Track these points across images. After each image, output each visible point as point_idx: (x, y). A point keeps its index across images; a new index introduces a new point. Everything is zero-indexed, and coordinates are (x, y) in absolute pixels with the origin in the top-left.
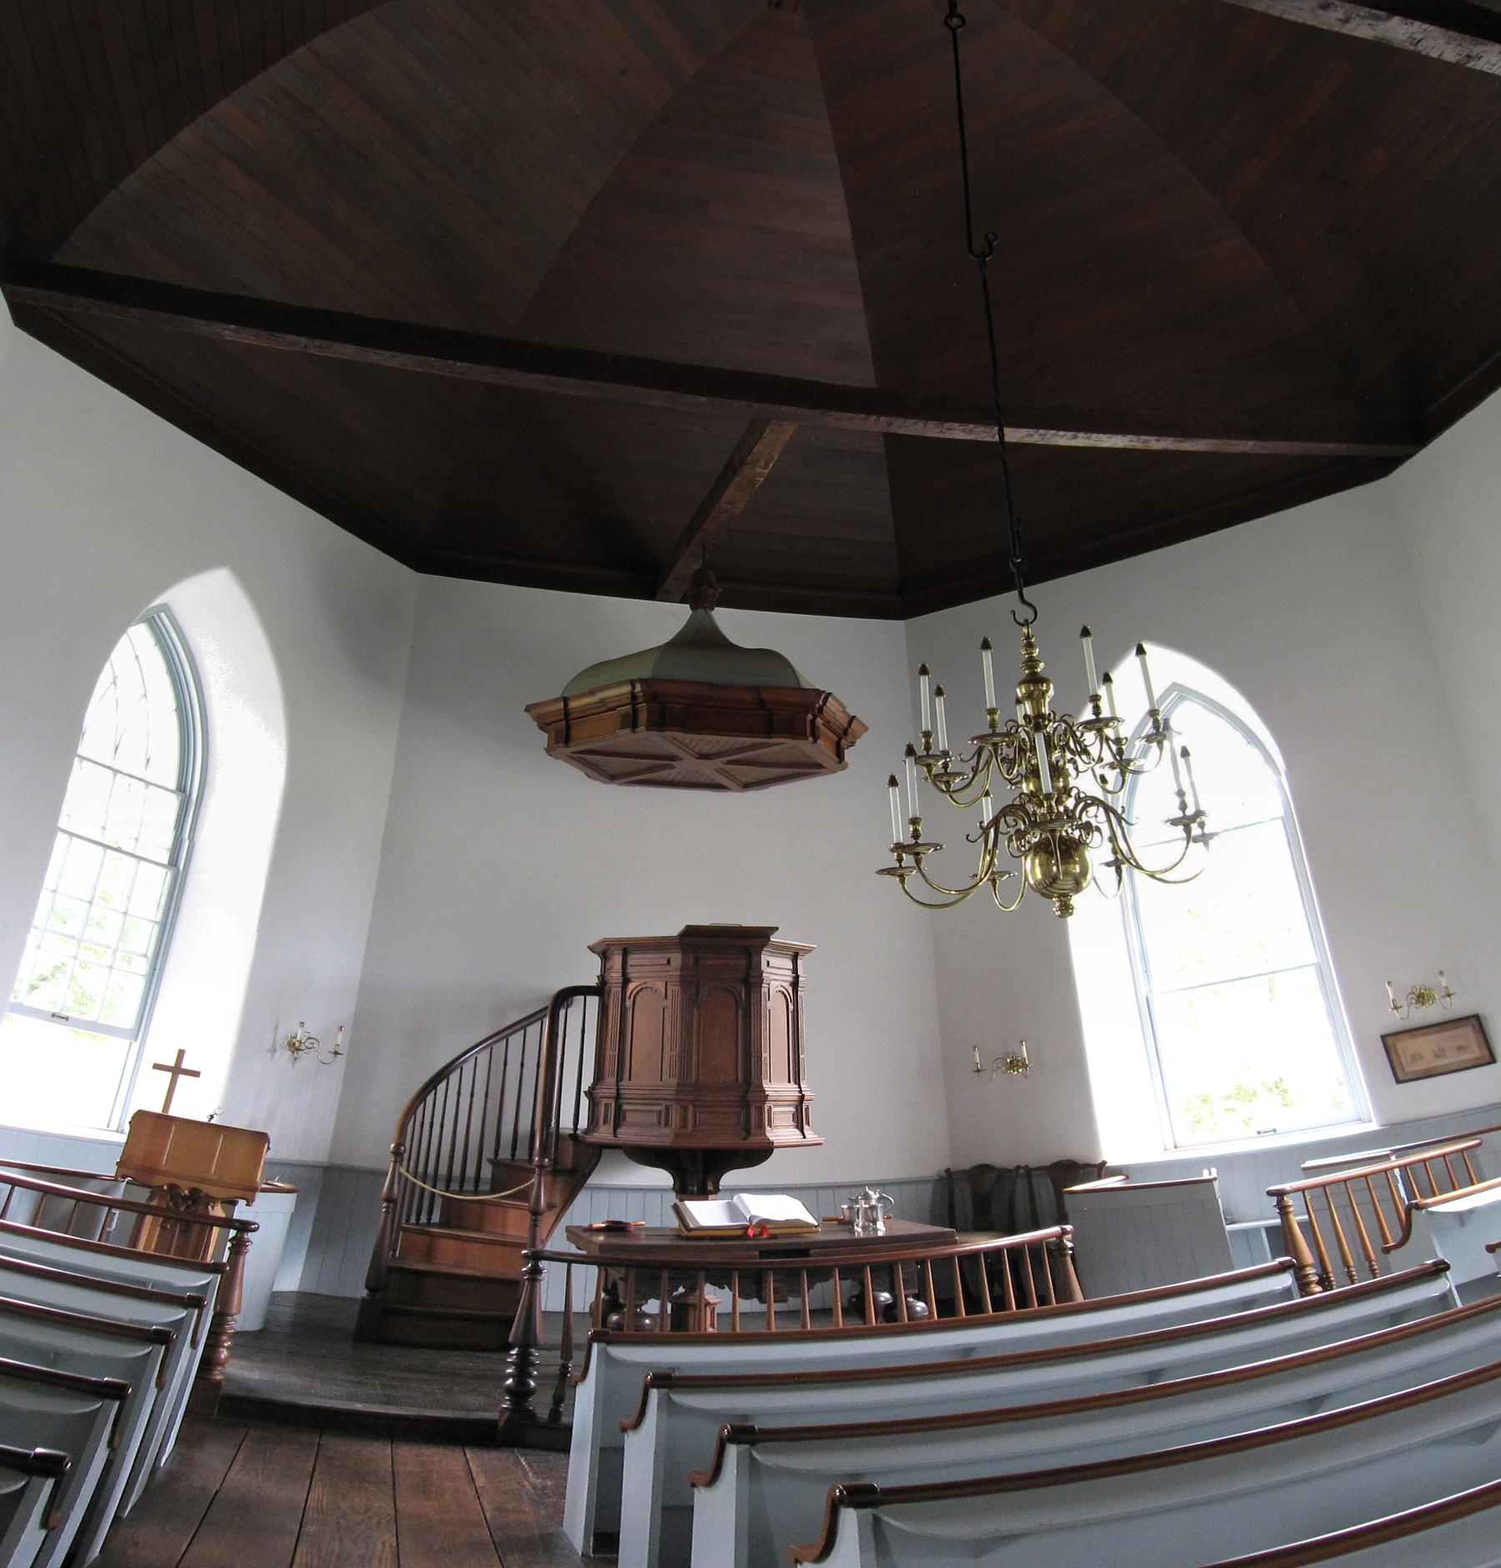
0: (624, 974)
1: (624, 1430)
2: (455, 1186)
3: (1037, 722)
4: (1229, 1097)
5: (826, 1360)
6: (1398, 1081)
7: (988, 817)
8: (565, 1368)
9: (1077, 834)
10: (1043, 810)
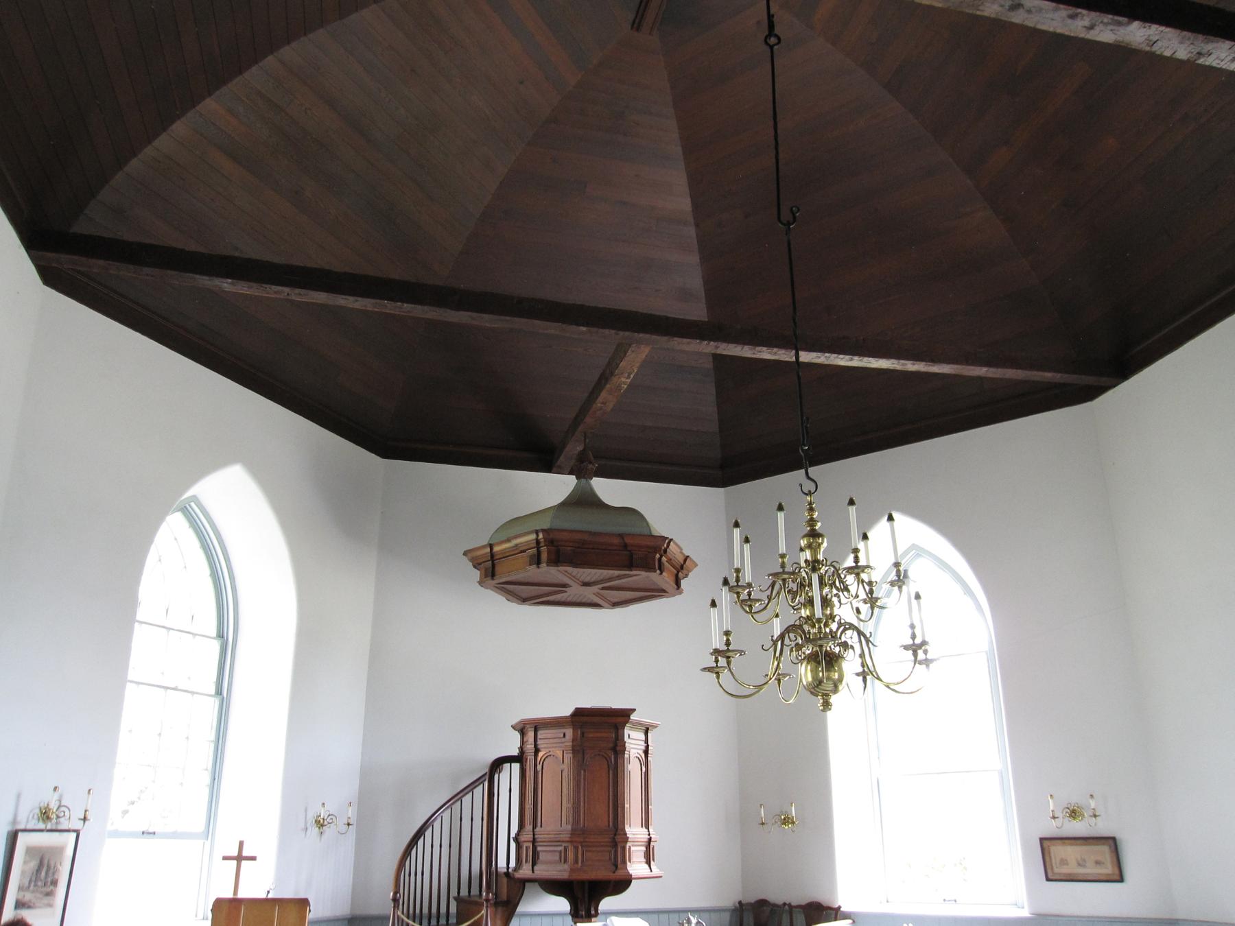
0: (536, 745)
3: (814, 565)
7: (777, 633)
9: (837, 650)
10: (815, 630)
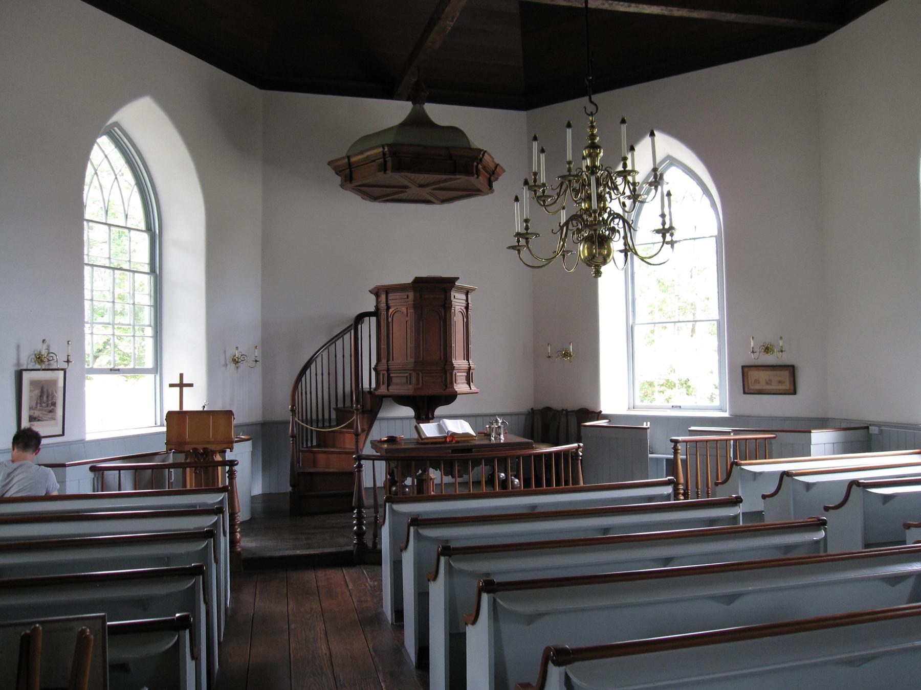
1: (401, 551)
2: (320, 425)
3: (593, 170)
4: (662, 385)
5: (478, 509)
6: (745, 393)
7: (563, 220)
8: (376, 517)
10: (592, 219)
